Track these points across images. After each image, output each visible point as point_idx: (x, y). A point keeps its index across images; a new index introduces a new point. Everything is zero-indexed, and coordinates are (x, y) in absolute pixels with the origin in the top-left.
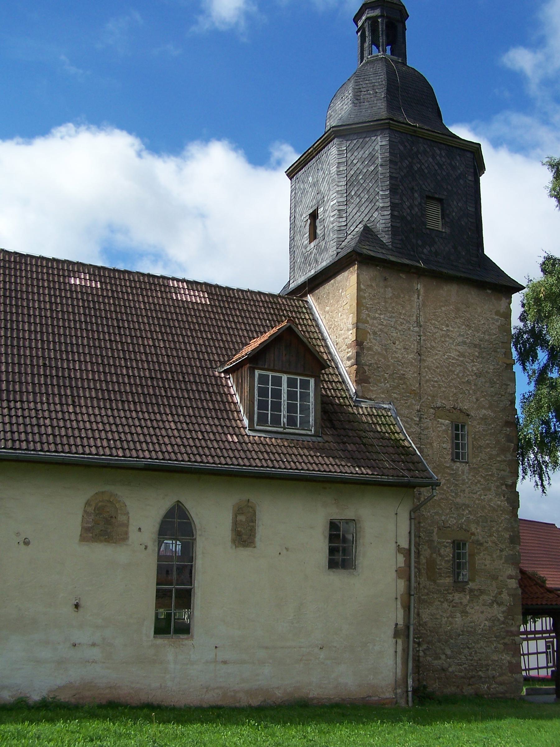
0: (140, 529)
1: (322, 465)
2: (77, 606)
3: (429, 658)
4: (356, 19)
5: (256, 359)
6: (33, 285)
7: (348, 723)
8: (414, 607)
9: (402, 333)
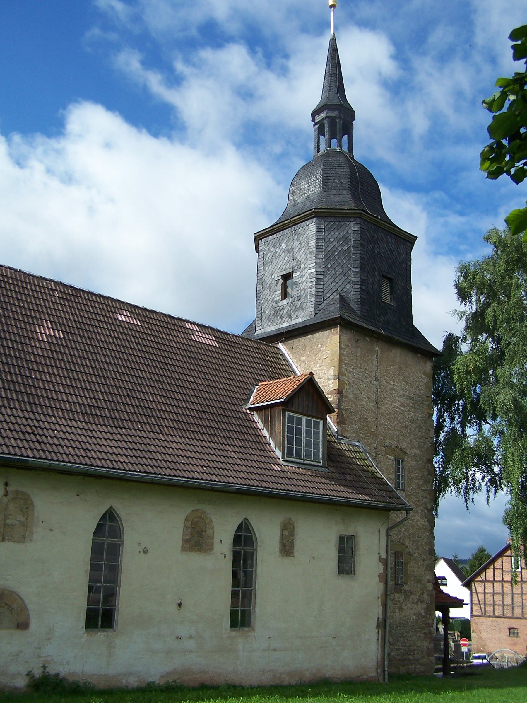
0: (221, 541)
4: (314, 114)
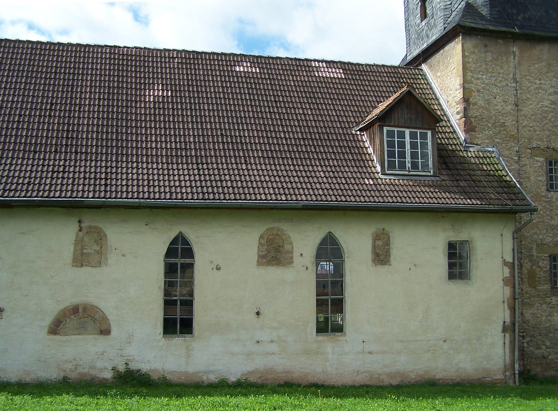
0: (301, 254)
1: (440, 199)
2: (258, 313)
3: (531, 348)
5: (384, 118)
6: (208, 75)
7: (467, 397)
8: (519, 308)
9: (501, 89)
